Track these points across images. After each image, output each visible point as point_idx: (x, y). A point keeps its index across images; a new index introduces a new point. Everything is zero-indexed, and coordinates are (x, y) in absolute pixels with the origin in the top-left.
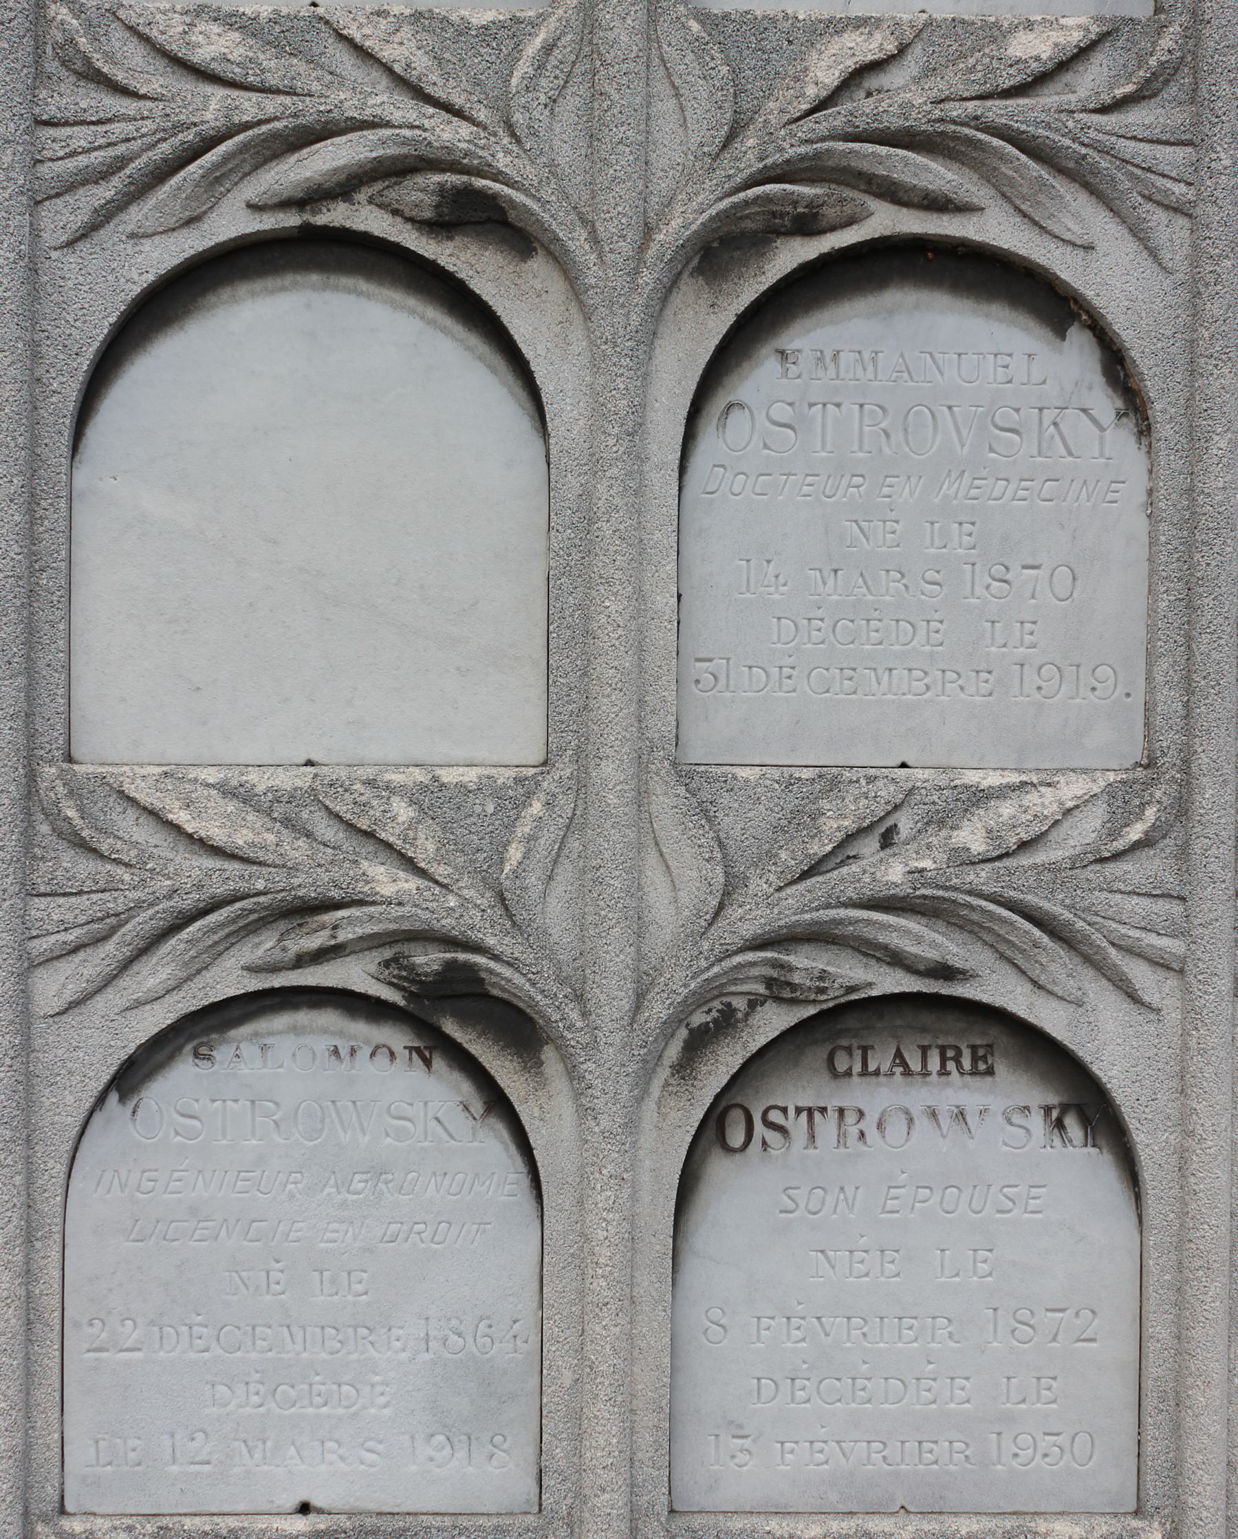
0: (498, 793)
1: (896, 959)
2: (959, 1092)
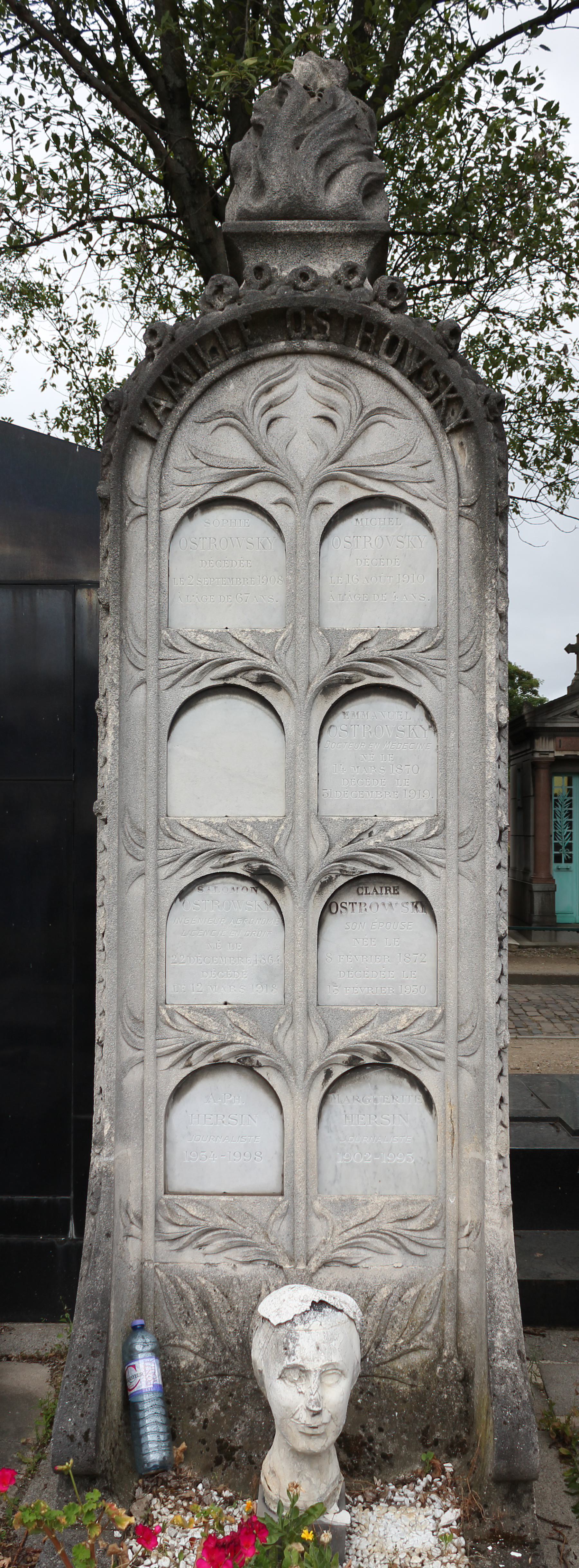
0: (273, 823)
1: (372, 865)
2: (390, 898)
